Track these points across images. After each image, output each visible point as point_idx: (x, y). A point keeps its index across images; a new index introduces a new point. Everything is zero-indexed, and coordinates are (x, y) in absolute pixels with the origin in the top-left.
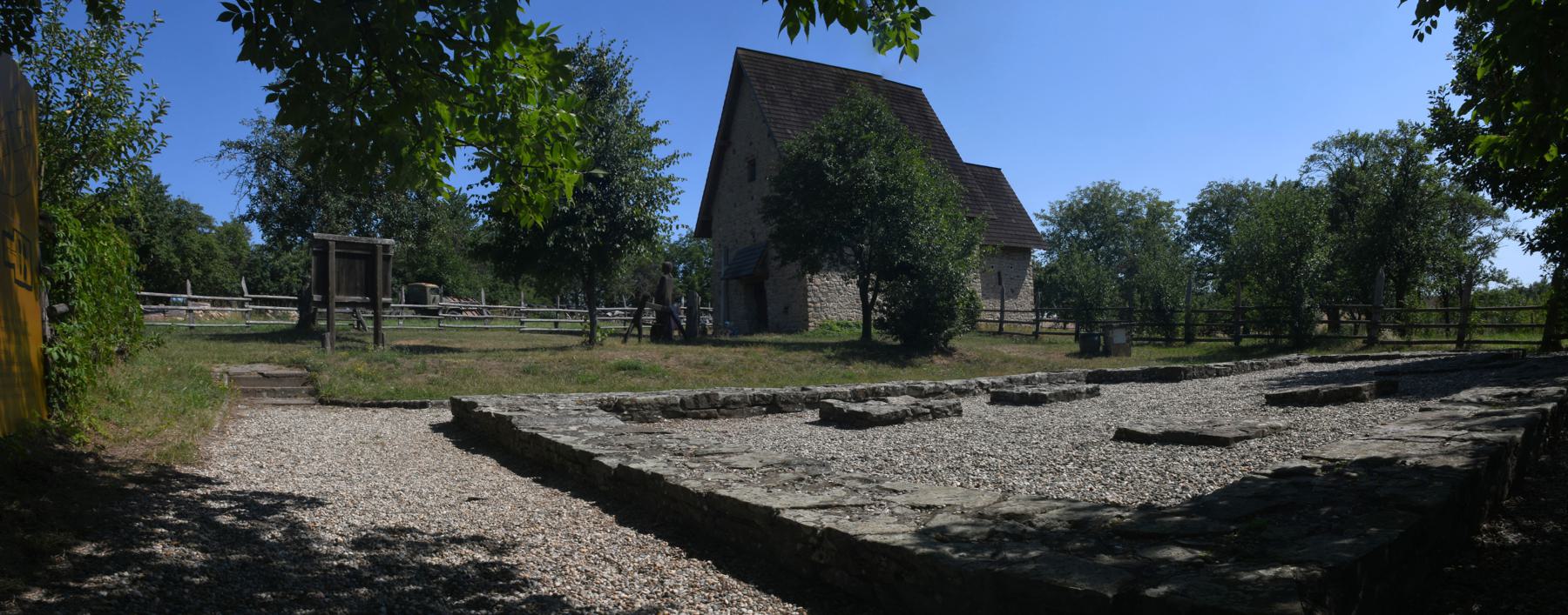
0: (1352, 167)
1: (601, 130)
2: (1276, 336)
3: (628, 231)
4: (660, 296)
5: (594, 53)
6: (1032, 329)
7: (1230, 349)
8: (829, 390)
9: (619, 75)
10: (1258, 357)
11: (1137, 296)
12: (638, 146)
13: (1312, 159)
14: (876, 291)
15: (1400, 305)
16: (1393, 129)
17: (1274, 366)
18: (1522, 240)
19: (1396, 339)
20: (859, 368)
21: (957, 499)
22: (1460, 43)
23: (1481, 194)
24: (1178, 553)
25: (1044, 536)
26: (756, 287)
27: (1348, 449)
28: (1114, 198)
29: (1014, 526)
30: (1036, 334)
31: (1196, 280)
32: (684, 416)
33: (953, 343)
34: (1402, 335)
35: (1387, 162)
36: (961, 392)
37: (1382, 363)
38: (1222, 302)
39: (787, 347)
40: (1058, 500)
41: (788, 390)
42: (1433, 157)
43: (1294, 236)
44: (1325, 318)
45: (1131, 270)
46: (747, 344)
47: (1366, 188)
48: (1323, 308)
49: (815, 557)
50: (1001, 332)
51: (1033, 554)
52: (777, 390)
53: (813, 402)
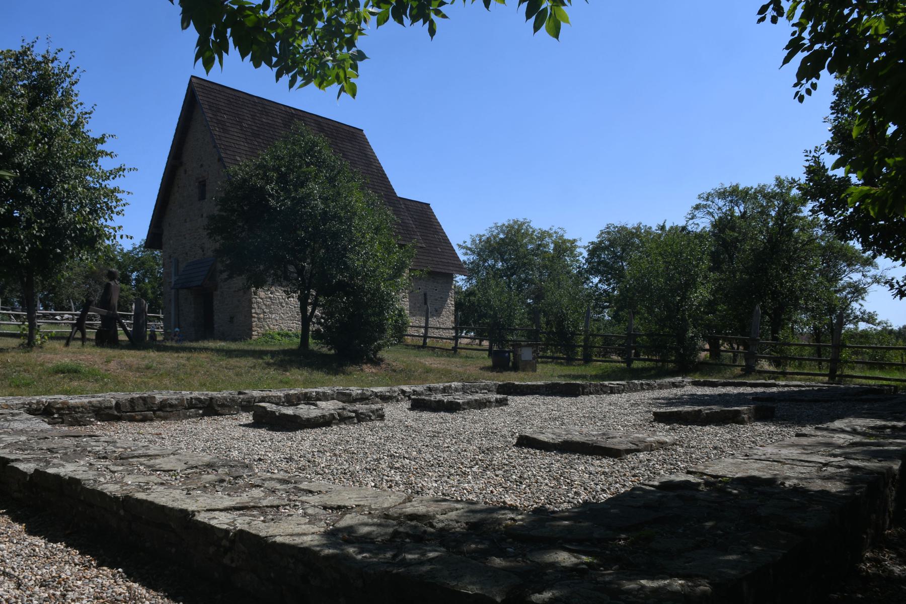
0: (732, 215)
1: (45, 136)
2: (664, 361)
3: (69, 237)
4: (105, 302)
5: (39, 59)
6: (451, 344)
7: (622, 370)
8: (264, 394)
9: (64, 85)
10: (648, 378)
11: (543, 319)
12: (83, 156)
13: (697, 207)
14: (315, 305)
15: (775, 339)
16: (770, 183)
17: (661, 387)
18: (892, 286)
19: (772, 369)
20: (296, 374)
21: (366, 499)
22: (836, 107)
23: (851, 243)
24: (564, 558)
25: (444, 536)
26: (205, 297)
27: (728, 467)
28: (526, 234)
29: (415, 527)
30: (455, 349)
31: (594, 308)
32: (118, 419)
33: (381, 354)
34: (777, 366)
35: (764, 212)
36: (385, 399)
37: (759, 390)
38: (616, 328)
39: (230, 353)
40: (457, 501)
41: (225, 393)
42: (806, 210)
43: (679, 273)
44: (707, 346)
45: (538, 297)
46: (190, 350)
47: (745, 234)
48: (705, 338)
49: (226, 560)
50: (424, 346)
51: (431, 555)
52: (215, 394)
53: (247, 406)
